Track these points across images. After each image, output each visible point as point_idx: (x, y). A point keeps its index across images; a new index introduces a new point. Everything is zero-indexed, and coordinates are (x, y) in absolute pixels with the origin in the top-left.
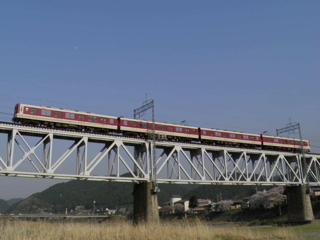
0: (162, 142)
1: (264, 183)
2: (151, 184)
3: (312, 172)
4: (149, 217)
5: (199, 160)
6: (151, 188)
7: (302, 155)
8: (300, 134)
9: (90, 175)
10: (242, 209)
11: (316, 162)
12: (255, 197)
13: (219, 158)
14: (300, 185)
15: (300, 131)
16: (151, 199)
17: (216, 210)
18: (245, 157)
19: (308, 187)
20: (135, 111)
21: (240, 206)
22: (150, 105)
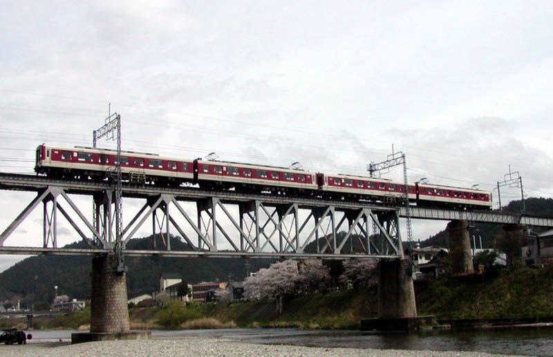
20: (95, 132)
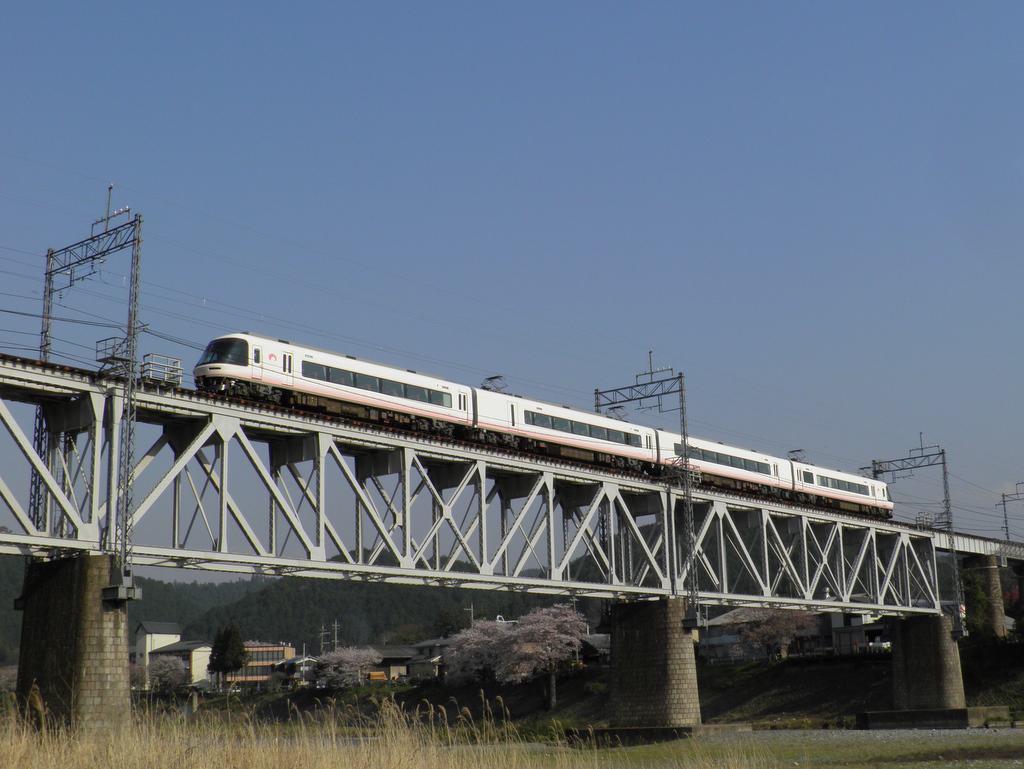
0: (161, 395)
1: (539, 586)
2: (106, 565)
3: (704, 556)
4: (89, 702)
5: (208, 467)
6: (106, 581)
7: (682, 493)
8: (683, 413)
9: (495, 574)
10: (412, 682)
11: (616, 501)
12: (466, 640)
13: (381, 478)
14: (664, 599)
15: (682, 400)
16: (101, 628)
17: (315, 682)
18: (547, 491)
19: (692, 609)
20: (51, 254)
21: (403, 670)
22: (125, 235)
